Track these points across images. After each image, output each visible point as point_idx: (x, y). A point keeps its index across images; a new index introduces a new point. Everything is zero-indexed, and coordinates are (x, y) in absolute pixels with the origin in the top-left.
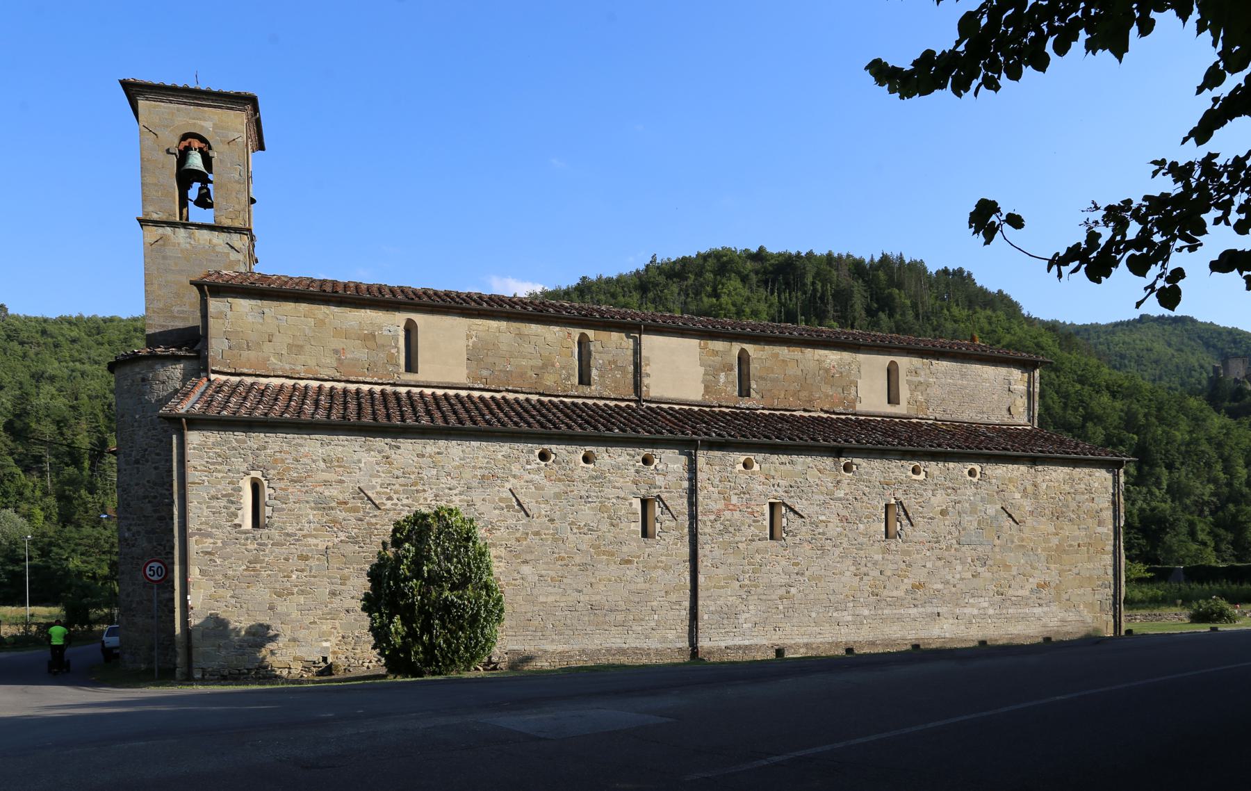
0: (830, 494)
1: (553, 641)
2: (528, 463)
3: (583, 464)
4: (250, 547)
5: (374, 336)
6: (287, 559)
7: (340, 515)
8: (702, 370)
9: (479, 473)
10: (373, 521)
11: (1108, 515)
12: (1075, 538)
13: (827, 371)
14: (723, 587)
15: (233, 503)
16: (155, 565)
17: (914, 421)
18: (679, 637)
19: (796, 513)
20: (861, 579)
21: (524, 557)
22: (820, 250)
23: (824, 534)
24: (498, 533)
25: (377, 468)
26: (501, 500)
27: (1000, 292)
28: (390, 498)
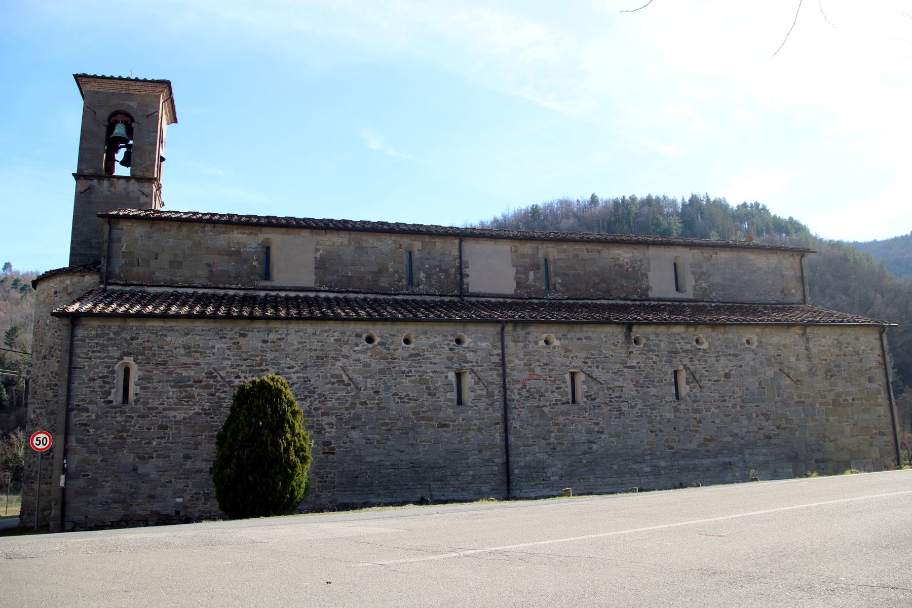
0: (623, 363)
1: (379, 495)
2: (357, 345)
3: (404, 345)
4: (119, 419)
5: (240, 252)
6: (149, 429)
7: (195, 391)
8: (514, 270)
9: (313, 354)
10: (223, 395)
11: (879, 373)
12: (849, 393)
13: (621, 266)
14: (531, 445)
15: (108, 383)
16: (42, 436)
17: (701, 304)
18: (493, 490)
19: (594, 379)
20: (657, 435)
21: (352, 423)
22: (641, 195)
23: (620, 397)
24: (330, 404)
25: (228, 352)
26: (332, 376)
27: (791, 218)
28: (238, 377)
